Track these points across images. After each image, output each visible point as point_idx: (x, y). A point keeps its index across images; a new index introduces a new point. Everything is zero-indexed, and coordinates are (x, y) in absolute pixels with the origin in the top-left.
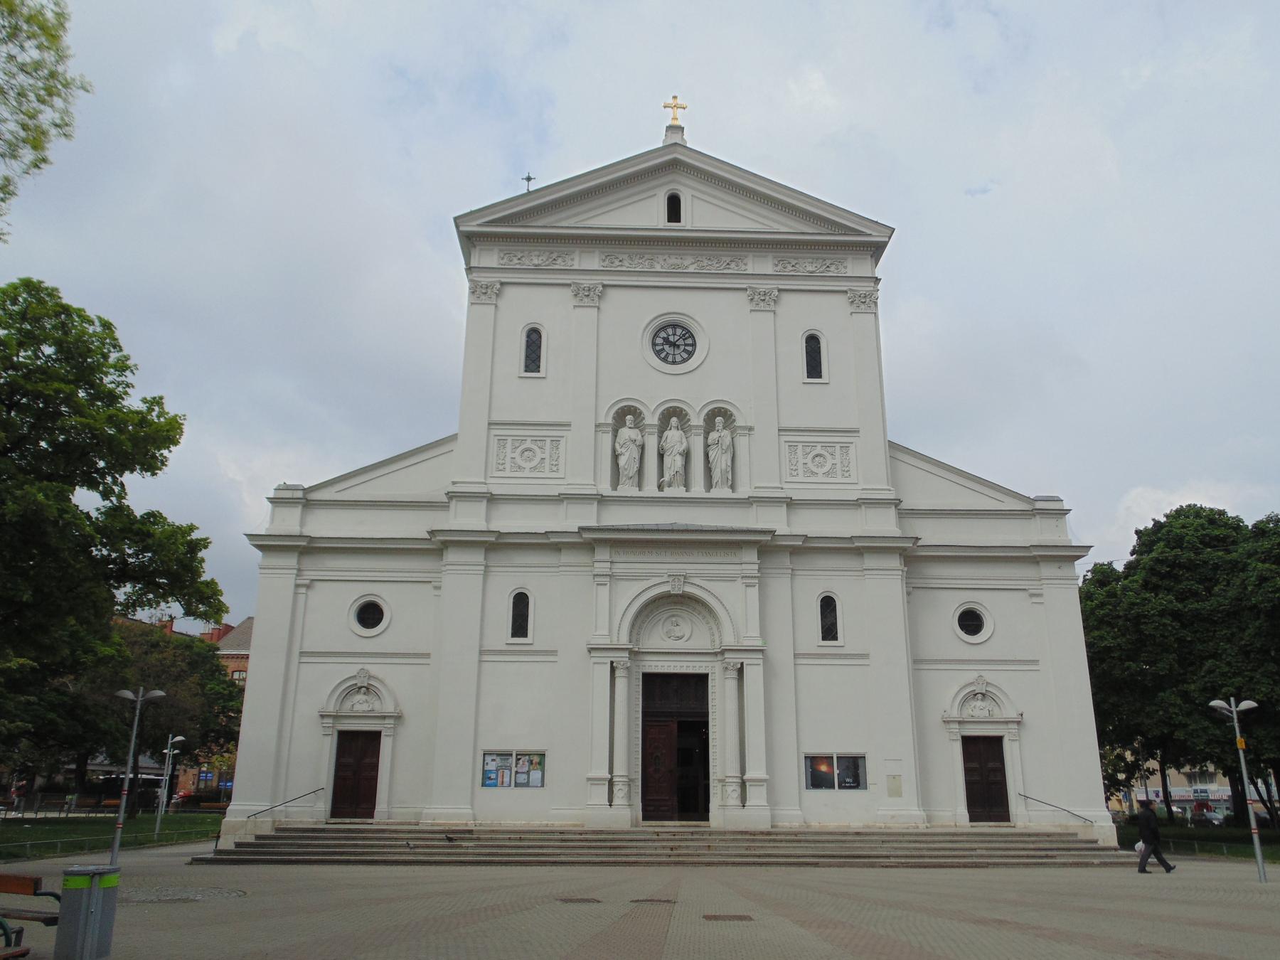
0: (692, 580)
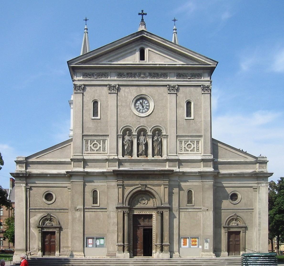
0: (148, 186)
